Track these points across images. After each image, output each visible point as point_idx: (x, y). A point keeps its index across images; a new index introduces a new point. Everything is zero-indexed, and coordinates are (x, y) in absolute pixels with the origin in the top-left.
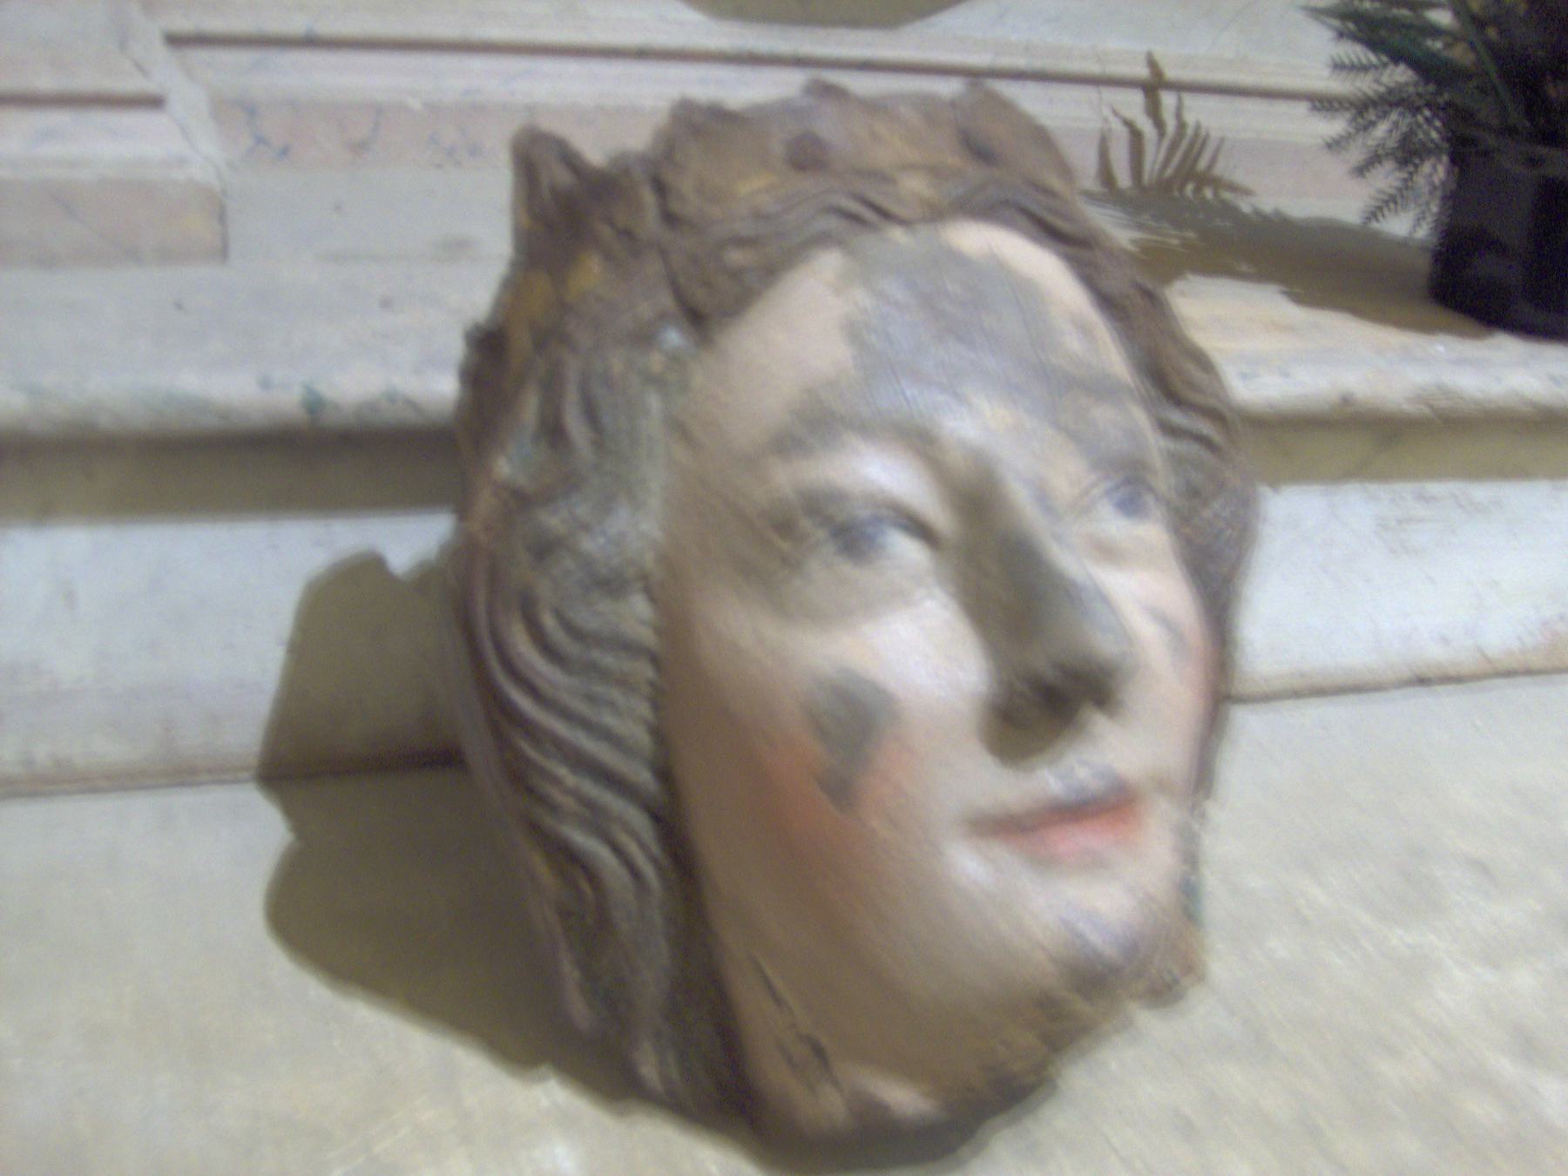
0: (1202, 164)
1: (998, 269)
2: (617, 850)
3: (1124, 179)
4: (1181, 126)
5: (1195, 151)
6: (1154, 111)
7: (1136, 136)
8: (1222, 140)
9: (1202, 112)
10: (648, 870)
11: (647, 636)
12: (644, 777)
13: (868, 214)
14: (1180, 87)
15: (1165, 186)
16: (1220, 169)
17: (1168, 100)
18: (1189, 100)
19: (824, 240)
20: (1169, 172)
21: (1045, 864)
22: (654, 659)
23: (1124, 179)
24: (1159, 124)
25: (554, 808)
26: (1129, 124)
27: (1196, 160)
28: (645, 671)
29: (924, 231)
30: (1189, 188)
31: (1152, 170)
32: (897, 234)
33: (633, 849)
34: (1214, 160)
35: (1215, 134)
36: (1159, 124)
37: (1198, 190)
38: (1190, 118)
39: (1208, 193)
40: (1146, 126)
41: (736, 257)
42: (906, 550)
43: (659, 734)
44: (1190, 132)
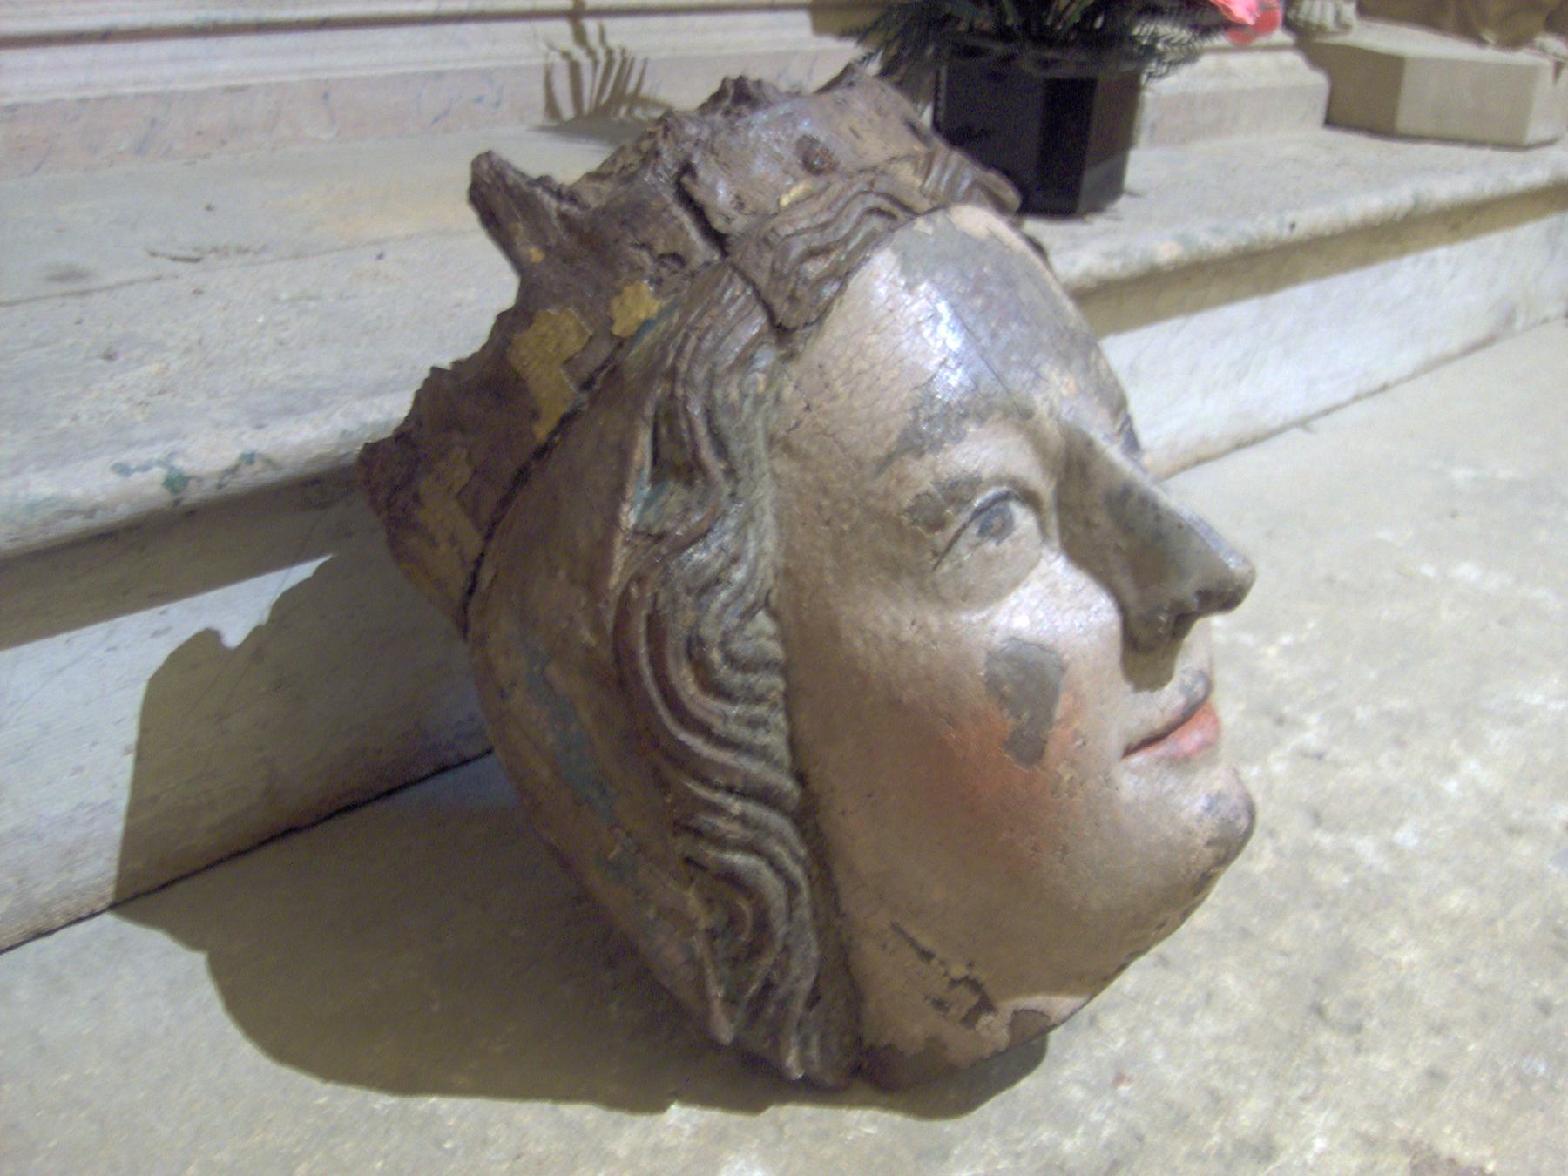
0: (631, 87)
1: (681, 227)
2: (773, 862)
3: (568, 112)
4: (609, 52)
5: (625, 76)
6: (580, 37)
7: (574, 68)
8: (646, 61)
9: (621, 33)
10: (797, 872)
11: (775, 650)
12: (788, 784)
13: (896, 210)
14: (599, 13)
15: (602, 111)
16: (645, 90)
17: (591, 25)
18: (611, 24)
19: (873, 242)
20: (605, 98)
21: (1182, 763)
22: (784, 670)
23: (568, 112)
24: (591, 53)
25: (721, 843)
26: (566, 55)
27: (625, 86)
28: (779, 683)
29: (939, 217)
30: (623, 111)
31: (591, 99)
32: (921, 224)
33: (788, 861)
34: (639, 84)
35: (640, 58)
36: (591, 53)
37: (630, 111)
38: (613, 42)
39: (638, 112)
40: (579, 54)
41: (814, 268)
42: (1023, 519)
43: (793, 743)
44: (618, 57)
